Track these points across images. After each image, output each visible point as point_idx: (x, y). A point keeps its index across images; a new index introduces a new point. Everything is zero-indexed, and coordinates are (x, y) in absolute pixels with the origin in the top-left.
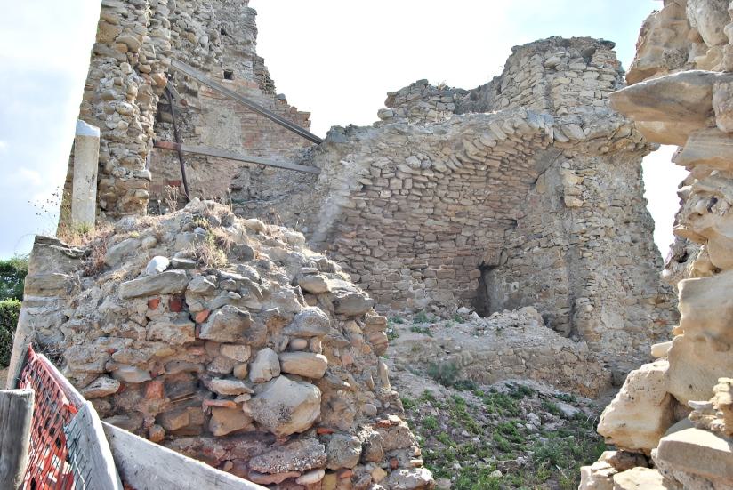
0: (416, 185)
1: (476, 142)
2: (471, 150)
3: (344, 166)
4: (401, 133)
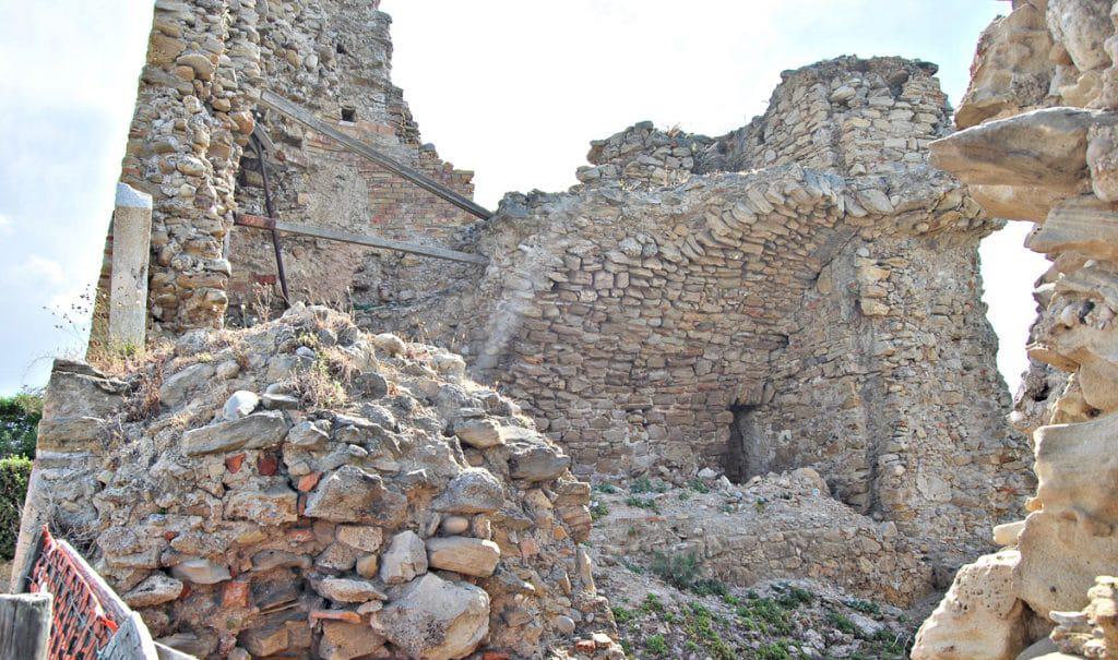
1: (726, 217)
2: (720, 229)
3: (525, 253)
4: (611, 203)
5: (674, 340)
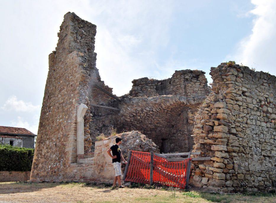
0: (147, 115)
1: (165, 104)
2: (164, 106)
3: (128, 109)
4: (145, 101)
5: (153, 126)
